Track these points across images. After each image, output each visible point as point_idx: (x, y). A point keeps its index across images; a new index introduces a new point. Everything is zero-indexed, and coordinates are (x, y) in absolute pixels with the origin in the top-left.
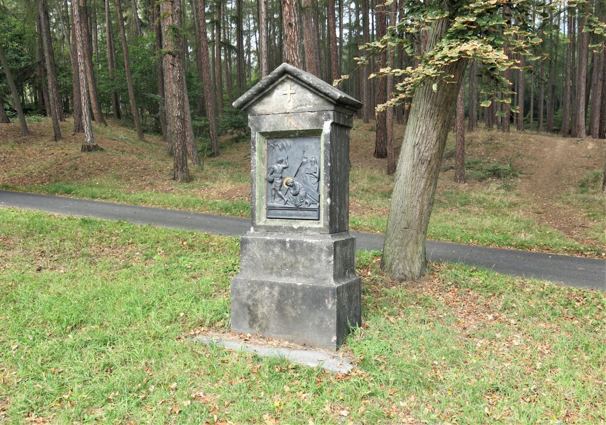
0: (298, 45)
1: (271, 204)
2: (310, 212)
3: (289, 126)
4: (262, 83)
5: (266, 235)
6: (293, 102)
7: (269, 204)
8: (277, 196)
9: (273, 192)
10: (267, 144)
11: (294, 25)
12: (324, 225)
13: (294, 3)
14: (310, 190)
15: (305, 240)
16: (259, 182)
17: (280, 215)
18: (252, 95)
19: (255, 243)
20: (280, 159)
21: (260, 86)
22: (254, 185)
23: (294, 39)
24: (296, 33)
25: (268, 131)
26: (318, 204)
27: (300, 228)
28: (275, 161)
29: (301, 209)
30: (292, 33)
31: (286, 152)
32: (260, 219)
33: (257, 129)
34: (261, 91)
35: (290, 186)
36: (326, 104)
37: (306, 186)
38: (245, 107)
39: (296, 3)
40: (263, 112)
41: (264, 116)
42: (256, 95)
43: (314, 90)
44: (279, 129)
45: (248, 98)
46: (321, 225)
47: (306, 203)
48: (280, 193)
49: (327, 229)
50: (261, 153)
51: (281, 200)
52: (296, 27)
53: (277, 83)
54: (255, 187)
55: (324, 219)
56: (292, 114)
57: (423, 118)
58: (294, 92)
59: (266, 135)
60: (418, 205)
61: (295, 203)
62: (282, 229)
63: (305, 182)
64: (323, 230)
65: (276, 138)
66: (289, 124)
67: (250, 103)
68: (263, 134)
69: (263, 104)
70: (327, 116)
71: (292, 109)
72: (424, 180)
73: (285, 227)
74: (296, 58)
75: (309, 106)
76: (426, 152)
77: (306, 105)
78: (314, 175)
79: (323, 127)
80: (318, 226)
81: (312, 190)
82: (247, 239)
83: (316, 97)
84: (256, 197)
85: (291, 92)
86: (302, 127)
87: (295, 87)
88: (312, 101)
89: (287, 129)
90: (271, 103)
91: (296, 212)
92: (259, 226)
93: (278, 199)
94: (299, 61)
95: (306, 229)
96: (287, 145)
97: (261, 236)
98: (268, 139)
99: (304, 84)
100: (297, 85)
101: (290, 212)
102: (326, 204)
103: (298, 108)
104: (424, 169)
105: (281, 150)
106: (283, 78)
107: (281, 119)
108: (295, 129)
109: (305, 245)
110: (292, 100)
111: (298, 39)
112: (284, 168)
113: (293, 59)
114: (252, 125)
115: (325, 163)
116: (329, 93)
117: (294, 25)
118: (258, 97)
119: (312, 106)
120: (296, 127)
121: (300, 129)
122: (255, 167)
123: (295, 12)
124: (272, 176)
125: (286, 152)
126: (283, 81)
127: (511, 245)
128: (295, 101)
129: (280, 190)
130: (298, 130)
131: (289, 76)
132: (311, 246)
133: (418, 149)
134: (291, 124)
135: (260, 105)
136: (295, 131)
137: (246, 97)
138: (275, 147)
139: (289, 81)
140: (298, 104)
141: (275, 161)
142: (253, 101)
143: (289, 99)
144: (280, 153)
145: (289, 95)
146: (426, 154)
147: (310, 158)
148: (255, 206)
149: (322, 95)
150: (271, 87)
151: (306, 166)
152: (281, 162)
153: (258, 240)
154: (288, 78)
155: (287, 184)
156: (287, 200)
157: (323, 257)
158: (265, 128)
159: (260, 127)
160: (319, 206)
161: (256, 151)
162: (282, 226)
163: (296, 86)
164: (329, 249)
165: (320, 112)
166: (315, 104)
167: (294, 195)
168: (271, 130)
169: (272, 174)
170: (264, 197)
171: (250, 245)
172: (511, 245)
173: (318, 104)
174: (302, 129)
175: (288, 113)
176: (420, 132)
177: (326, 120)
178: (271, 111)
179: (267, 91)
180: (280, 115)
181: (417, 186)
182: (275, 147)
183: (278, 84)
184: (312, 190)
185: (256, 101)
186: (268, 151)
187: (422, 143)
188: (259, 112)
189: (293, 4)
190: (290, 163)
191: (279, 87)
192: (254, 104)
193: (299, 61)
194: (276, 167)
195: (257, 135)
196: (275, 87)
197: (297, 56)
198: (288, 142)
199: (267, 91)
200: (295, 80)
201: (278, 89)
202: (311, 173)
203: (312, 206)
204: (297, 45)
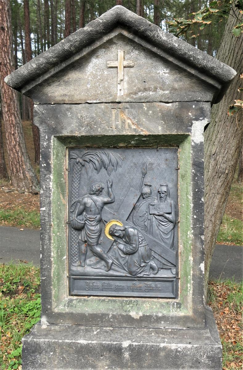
0: (10, 49)
1: (77, 269)
2: (159, 284)
3: (120, 127)
4: (70, 41)
5: (76, 333)
6: (128, 83)
7: (74, 268)
8: (89, 253)
9: (83, 247)
10: (70, 159)
11: (6, 29)
12: (195, 311)
13: (6, 9)
14: (158, 244)
15: (162, 345)
16: (56, 230)
17: (97, 289)
18: (47, 63)
19: (55, 352)
20: (96, 187)
21: (67, 47)
22: (47, 237)
23: (7, 43)
24: (8, 38)
25: (77, 134)
26: (174, 271)
27: (146, 319)
28: (85, 188)
29: (141, 279)
30: (4, 37)
31: (109, 175)
32: (58, 300)
33: (53, 131)
34: (65, 56)
35: (119, 237)
36: (196, 89)
37: (151, 237)
38: (30, 87)
39: (8, 9)
40: (67, 99)
41: (68, 106)
42: (54, 65)
43: (176, 62)
44: (99, 132)
45: (38, 68)
46: (187, 311)
47: (152, 268)
48: (98, 249)
49: (200, 320)
50: (59, 175)
51: (98, 263)
52: (8, 31)
53: (98, 44)
54: (50, 239)
55: (194, 301)
56: (127, 105)
57: (223, 122)
58: (132, 64)
59: (70, 143)
60: (211, 225)
61: (129, 268)
62: (109, 321)
63: (148, 229)
64: (193, 320)
65: (88, 147)
66: (119, 123)
67: (41, 80)
68: (63, 140)
69: (67, 83)
70: (199, 112)
71: (129, 95)
72: (219, 196)
73: (114, 317)
74: (8, 61)
75: (161, 92)
76: (224, 163)
77: (155, 89)
78: (166, 218)
79: (190, 131)
80: (181, 313)
81: (163, 244)
82: (38, 345)
83: (177, 76)
84: (52, 259)
85: (125, 63)
86: (148, 130)
87: (132, 54)
88: (168, 82)
89: (116, 133)
90: (82, 82)
91: (130, 284)
92: (60, 316)
93: (94, 259)
94: (12, 64)
95: (158, 319)
96: (110, 161)
97: (66, 337)
98: (71, 149)
99: (155, 49)
100: (137, 52)
101: (118, 283)
102: (198, 273)
104: (219, 184)
105: (97, 170)
106: (112, 35)
107: (104, 113)
108: (134, 133)
109: (162, 354)
110: (126, 78)
111: (10, 43)
112: (105, 204)
113: (5, 62)
114: (42, 122)
115: (194, 198)
116: (213, 68)
117: (6, 29)
118: (57, 69)
119: (167, 92)
120: (135, 130)
121: (142, 133)
122: (50, 203)
123: (8, 17)
124: (80, 217)
125: (109, 175)
126: (110, 42)
127: (228, 240)
128: (133, 82)
129: (98, 244)
130: (139, 136)
131: (125, 33)
132: (177, 356)
133: (215, 160)
134: (123, 122)
135: (59, 85)
136: (133, 136)
137: (35, 66)
138: (87, 165)
139: (120, 43)
140: (140, 86)
141: (85, 189)
142: (46, 76)
143: (120, 77)
144: (96, 176)
145: (121, 71)
146: (223, 166)
147: (156, 186)
148: (49, 277)
149: (193, 72)
150: (85, 53)
151: (149, 200)
152: (99, 192)
153: (61, 345)
154: (121, 37)
155: (112, 234)
156: (113, 263)
158: (69, 129)
159: (59, 127)
160: (177, 274)
161: (50, 172)
162: (108, 315)
163: (135, 53)
164: (213, 361)
165: (184, 104)
166: (174, 89)
167: (126, 254)
168: (84, 134)
169: (80, 214)
170: (65, 257)
171: (43, 356)
172: (228, 240)
173: (181, 89)
174: (147, 133)
175: (119, 103)
176: (218, 139)
177: (197, 119)
178: (84, 98)
179: (77, 58)
180: (103, 106)
181: (210, 202)
182: (87, 165)
183: (101, 47)
184: (163, 244)
185: (53, 76)
186: (71, 170)
187: (220, 152)
188: (59, 99)
189: (5, 10)
190: (118, 193)
191: (101, 52)
192: (48, 82)
193: (12, 64)
194: (88, 201)
195: (53, 142)
196: (93, 53)
197: (9, 60)
198: (113, 155)
199: (77, 58)
200: (136, 40)
201: (97, 57)
202: (161, 213)
203: (164, 274)
204: (9, 49)
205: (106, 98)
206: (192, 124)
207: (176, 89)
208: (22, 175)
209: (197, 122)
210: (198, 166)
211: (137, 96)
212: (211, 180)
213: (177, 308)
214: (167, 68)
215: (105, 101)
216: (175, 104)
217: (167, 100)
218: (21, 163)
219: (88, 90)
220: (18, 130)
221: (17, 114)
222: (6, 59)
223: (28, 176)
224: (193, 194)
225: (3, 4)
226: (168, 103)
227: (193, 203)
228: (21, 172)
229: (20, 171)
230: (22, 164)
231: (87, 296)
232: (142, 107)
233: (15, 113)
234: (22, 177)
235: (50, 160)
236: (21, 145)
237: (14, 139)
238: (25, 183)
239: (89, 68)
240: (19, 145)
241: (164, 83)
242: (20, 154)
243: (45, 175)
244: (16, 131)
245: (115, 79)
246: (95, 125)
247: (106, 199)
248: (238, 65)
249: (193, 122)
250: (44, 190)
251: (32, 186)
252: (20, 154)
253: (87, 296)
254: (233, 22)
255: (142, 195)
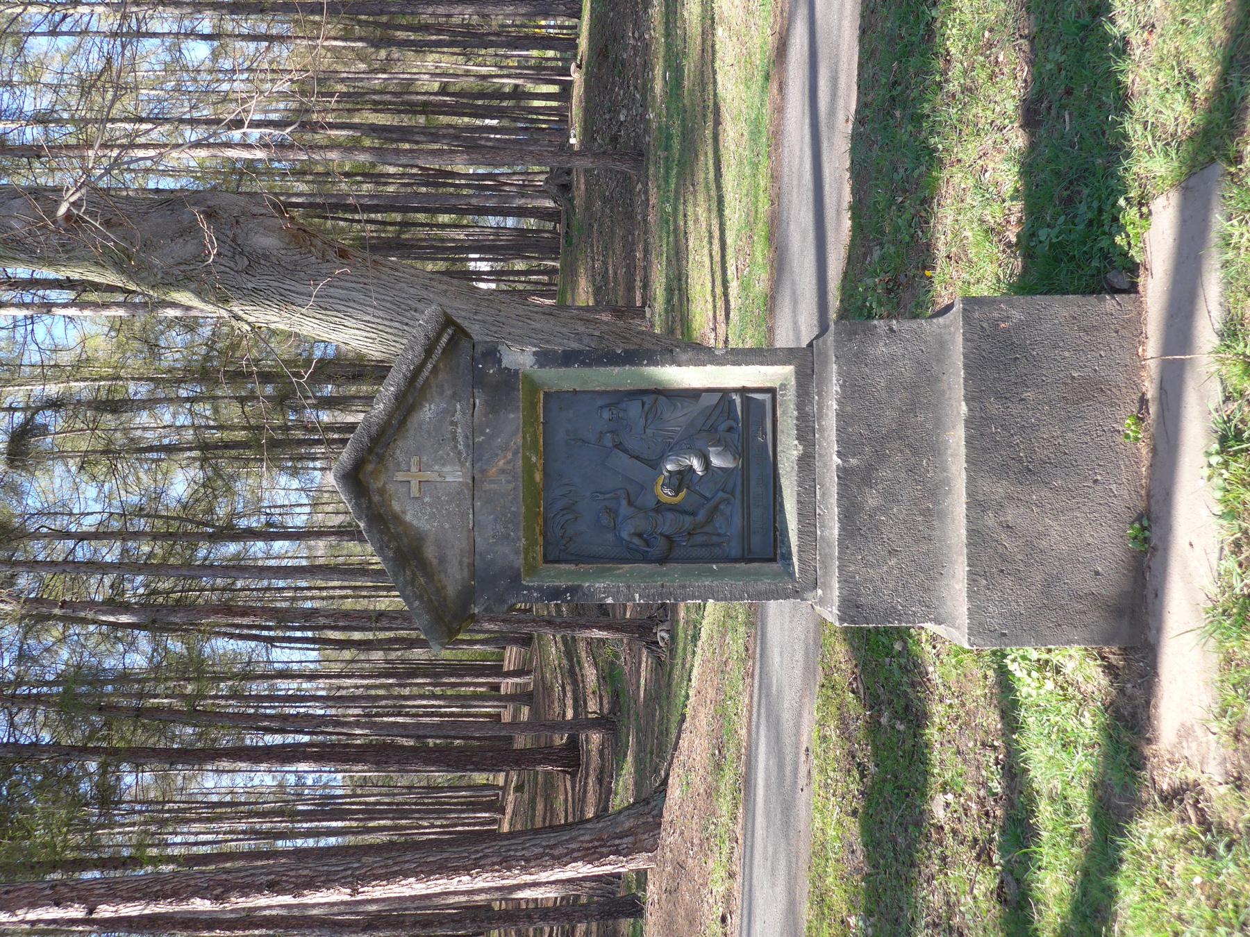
11: (273, 876)
30: (291, 883)
66: (503, 478)
71: (462, 464)
74: (349, 872)
77: (454, 424)
78: (650, 409)
86: (515, 433)
87: (401, 459)
93: (719, 521)
103: (461, 447)
134: (503, 471)
157: (880, 349)
161: (580, 586)
170: (715, 567)
177: (500, 361)
193: (356, 865)
197: (345, 870)
205: (465, 499)
206: (506, 368)
207: (455, 393)
208: (625, 840)
209: (504, 361)
210: (568, 359)
211: (464, 451)
212: (1157, 905)
213: (785, 389)
214: (422, 406)
215: (470, 500)
216: (476, 394)
217: (471, 406)
218: (596, 844)
219: (453, 527)
220: (516, 850)
221: (477, 852)
222: (343, 878)
223: (627, 825)
224: (611, 365)
225: (211, 883)
226: (474, 404)
227: (625, 365)
228: (617, 842)
229: (614, 845)
230: (598, 841)
231: (775, 532)
232: (480, 444)
233: (473, 857)
234: (630, 839)
235: (561, 586)
236: (552, 842)
237: (537, 858)
238: (644, 833)
239: (420, 525)
240: (552, 847)
241: (445, 411)
242: (573, 846)
243: (584, 594)
244: (519, 854)
245: (438, 485)
246: (506, 516)
247: (624, 503)
248: (396, 315)
249: (503, 366)
250: (607, 597)
251: (653, 817)
252: (573, 846)
253: (775, 532)
254: (315, 326)
255: (616, 446)
